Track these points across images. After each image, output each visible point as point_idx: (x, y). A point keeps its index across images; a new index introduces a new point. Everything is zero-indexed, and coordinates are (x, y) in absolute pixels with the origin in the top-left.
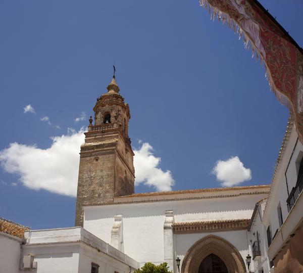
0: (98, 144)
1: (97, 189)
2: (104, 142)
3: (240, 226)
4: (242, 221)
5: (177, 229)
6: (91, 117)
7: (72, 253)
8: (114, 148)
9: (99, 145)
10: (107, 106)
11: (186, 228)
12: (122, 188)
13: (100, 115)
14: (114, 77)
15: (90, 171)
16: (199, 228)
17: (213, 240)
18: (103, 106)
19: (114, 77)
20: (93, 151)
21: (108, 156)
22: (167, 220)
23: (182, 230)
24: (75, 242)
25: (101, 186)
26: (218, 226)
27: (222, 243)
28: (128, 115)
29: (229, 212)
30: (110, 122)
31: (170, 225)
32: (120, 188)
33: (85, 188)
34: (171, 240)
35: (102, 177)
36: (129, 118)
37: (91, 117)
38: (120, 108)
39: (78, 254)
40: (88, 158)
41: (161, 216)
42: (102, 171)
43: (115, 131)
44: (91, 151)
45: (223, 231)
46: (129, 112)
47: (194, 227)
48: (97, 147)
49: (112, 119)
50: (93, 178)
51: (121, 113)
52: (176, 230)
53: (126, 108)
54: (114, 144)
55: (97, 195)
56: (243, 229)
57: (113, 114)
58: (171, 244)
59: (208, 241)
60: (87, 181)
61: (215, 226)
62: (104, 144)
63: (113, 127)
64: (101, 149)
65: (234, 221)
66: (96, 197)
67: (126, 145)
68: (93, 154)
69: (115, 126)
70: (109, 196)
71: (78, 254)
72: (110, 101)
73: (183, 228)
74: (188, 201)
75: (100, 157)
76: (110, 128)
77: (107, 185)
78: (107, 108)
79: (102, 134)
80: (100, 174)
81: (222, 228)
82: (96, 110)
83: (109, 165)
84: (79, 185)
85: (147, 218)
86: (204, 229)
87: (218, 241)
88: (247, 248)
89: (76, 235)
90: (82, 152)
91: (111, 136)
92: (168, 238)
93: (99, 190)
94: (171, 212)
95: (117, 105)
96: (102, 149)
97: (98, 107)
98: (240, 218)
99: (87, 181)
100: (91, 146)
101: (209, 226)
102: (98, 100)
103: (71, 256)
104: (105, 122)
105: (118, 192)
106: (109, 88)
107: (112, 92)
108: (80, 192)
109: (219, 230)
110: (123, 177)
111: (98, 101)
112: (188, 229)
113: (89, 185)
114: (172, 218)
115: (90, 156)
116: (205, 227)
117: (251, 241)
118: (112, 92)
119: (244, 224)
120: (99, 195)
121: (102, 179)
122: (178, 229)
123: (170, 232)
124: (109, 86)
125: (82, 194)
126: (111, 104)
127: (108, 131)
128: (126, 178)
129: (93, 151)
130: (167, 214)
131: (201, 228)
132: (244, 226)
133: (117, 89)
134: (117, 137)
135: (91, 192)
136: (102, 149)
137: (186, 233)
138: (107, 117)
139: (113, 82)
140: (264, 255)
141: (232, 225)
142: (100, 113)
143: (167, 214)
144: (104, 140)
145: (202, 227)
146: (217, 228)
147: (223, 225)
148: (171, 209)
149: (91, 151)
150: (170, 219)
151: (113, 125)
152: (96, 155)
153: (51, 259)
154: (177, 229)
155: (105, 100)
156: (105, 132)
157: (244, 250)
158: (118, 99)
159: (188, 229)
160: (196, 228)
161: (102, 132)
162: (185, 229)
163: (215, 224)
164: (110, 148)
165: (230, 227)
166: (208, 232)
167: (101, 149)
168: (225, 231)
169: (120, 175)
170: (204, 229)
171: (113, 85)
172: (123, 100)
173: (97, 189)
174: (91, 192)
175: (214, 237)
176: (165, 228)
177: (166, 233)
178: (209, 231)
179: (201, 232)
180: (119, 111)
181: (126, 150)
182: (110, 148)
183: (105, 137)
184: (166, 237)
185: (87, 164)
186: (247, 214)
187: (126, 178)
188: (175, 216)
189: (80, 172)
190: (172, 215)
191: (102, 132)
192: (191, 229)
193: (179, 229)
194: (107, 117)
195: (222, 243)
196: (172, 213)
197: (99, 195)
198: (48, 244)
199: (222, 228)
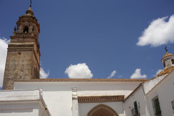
0: (21, 44)
1: (19, 72)
2: (25, 44)
3: (118, 99)
4: (120, 96)
5: (81, 100)
6: (15, 27)
7: (32, 109)
8: (32, 48)
9: (22, 45)
10: (26, 22)
11: (87, 99)
12: (35, 74)
13: (21, 28)
14: (31, 6)
15: (14, 61)
16: (94, 99)
17: (103, 107)
18: (23, 22)
19: (31, 6)
20: (17, 48)
21: (28, 52)
22: (73, 94)
23: (84, 100)
24: (35, 100)
25: (22, 71)
26: (106, 99)
27: (108, 109)
28: (39, 30)
29: (110, 91)
30: (27, 32)
31: (76, 97)
32: (34, 74)
33: (10, 72)
34: (77, 107)
35: (23, 65)
36: (39, 33)
37: (15, 27)
38: (35, 25)
39: (38, 110)
40: (13, 52)
41: (68, 91)
42: (23, 61)
43: (32, 38)
44: (15, 48)
45: (109, 102)
46: (39, 28)
47: (91, 99)
48: (20, 46)
49: (30, 31)
50: (16, 66)
51: (36, 28)
52: (80, 101)
53: (38, 25)
54: (32, 46)
55: (19, 77)
56: (120, 101)
57: (31, 28)
58: (77, 109)
59: (99, 108)
60: (11, 67)
61: (104, 99)
62: (25, 45)
63: (31, 35)
64: (22, 48)
65: (115, 96)
66: (18, 78)
67: (37, 48)
68: (17, 50)
69: (32, 35)
70: (28, 78)
71: (38, 110)
72: (29, 19)
73: (85, 99)
74: (88, 82)
75: (22, 52)
76: (29, 35)
77: (26, 71)
78: (26, 23)
79: (23, 38)
80: (21, 63)
81: (108, 100)
82: (18, 24)
83: (29, 58)
84: (6, 69)
85: (60, 92)
86: (97, 100)
87: (106, 108)
88: (123, 113)
89: (35, 95)
90: (9, 48)
91: (29, 41)
92: (75, 105)
93: (20, 73)
94: (75, 89)
95: (33, 22)
96: (24, 48)
97: (20, 22)
98: (116, 95)
99: (11, 67)
100: (15, 45)
101: (100, 99)
102: (20, 18)
103: (32, 111)
104: (24, 32)
105: (33, 76)
106: (27, 12)
107: (29, 14)
108: (6, 74)
109: (106, 101)
110: (35, 67)
111: (20, 18)
112: (87, 100)
113: (14, 70)
114: (76, 93)
115: (15, 51)
116: (98, 99)
117: (130, 108)
118: (29, 14)
119: (121, 98)
120: (21, 77)
121: (23, 67)
122: (81, 100)
123: (77, 101)
124: (27, 11)
125: (8, 75)
126: (29, 21)
127: (27, 37)
128: (36, 68)
129: (17, 48)
130: (73, 90)
131: (95, 100)
132: (120, 99)
133: (32, 14)
134: (34, 41)
135: (15, 74)
136: (24, 48)
137: (86, 102)
138: (26, 29)
139: (30, 9)
140: (145, 114)
141: (114, 98)
142: (21, 26)
143: (73, 90)
144: (25, 43)
145: (96, 99)
146: (105, 100)
147: (109, 98)
148: (75, 87)
149: (15, 48)
150: (75, 93)
151: (31, 34)
152: (19, 51)
153: (13, 114)
154: (81, 100)
155: (26, 18)
156: (25, 38)
157: (121, 114)
158: (33, 19)
159: (87, 100)
160: (92, 99)
161: (23, 37)
162: (86, 100)
163: (104, 98)
164: (29, 48)
165: (113, 99)
166: (99, 102)
167: (22, 48)
168: (110, 102)
169: (34, 66)
170: (97, 100)
171: (30, 11)
172: (37, 20)
173: (19, 72)
174: (15, 74)
175: (103, 105)
176: (73, 99)
177: (74, 102)
178: (100, 101)
179: (95, 102)
180: (34, 26)
181: (37, 51)
182: (29, 48)
183: (25, 41)
184: (74, 105)
185: (12, 56)
186: (126, 93)
187: (36, 68)
188: (78, 92)
189: (7, 61)
190: (76, 91)
191: (23, 37)
192: (89, 100)
193: (82, 100)
194: (26, 29)
195: (108, 109)
196: (76, 90)
197: (21, 77)
198: (12, 101)
199: (108, 100)
